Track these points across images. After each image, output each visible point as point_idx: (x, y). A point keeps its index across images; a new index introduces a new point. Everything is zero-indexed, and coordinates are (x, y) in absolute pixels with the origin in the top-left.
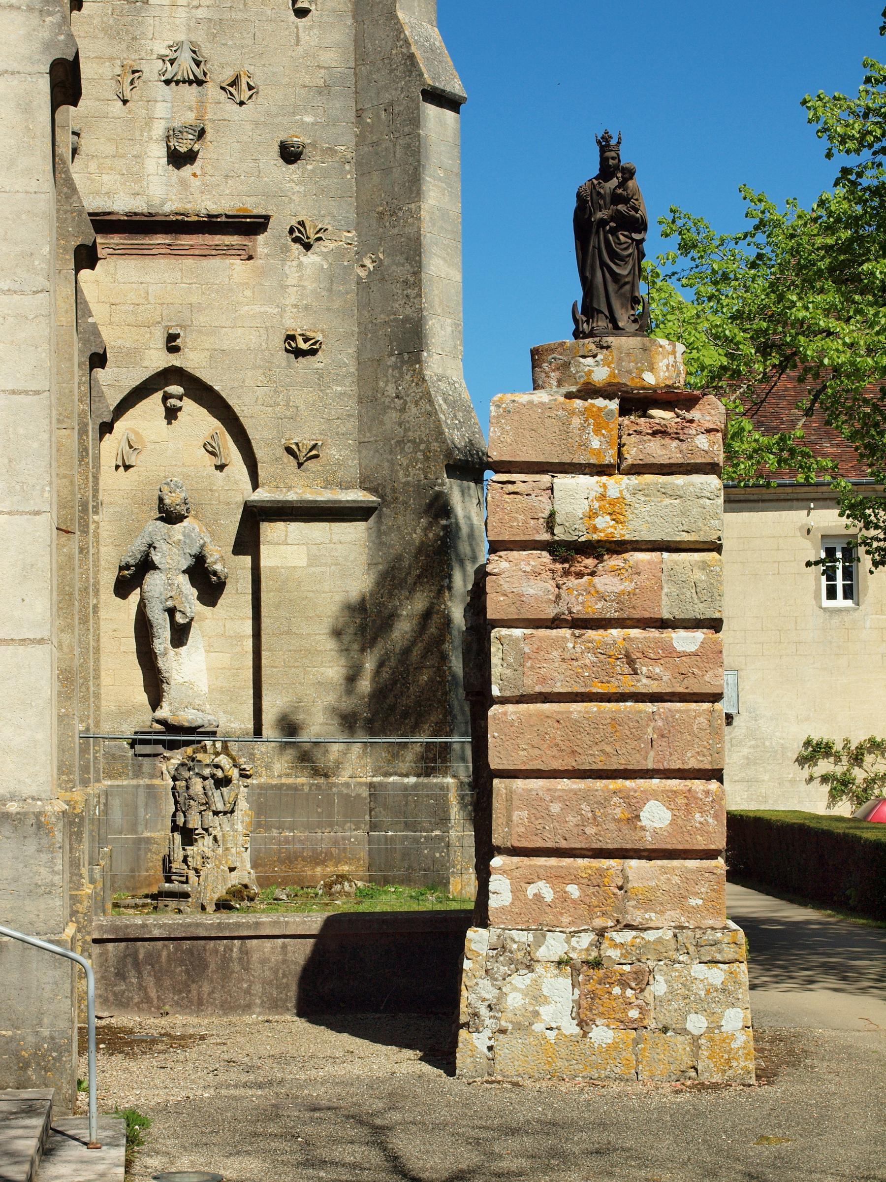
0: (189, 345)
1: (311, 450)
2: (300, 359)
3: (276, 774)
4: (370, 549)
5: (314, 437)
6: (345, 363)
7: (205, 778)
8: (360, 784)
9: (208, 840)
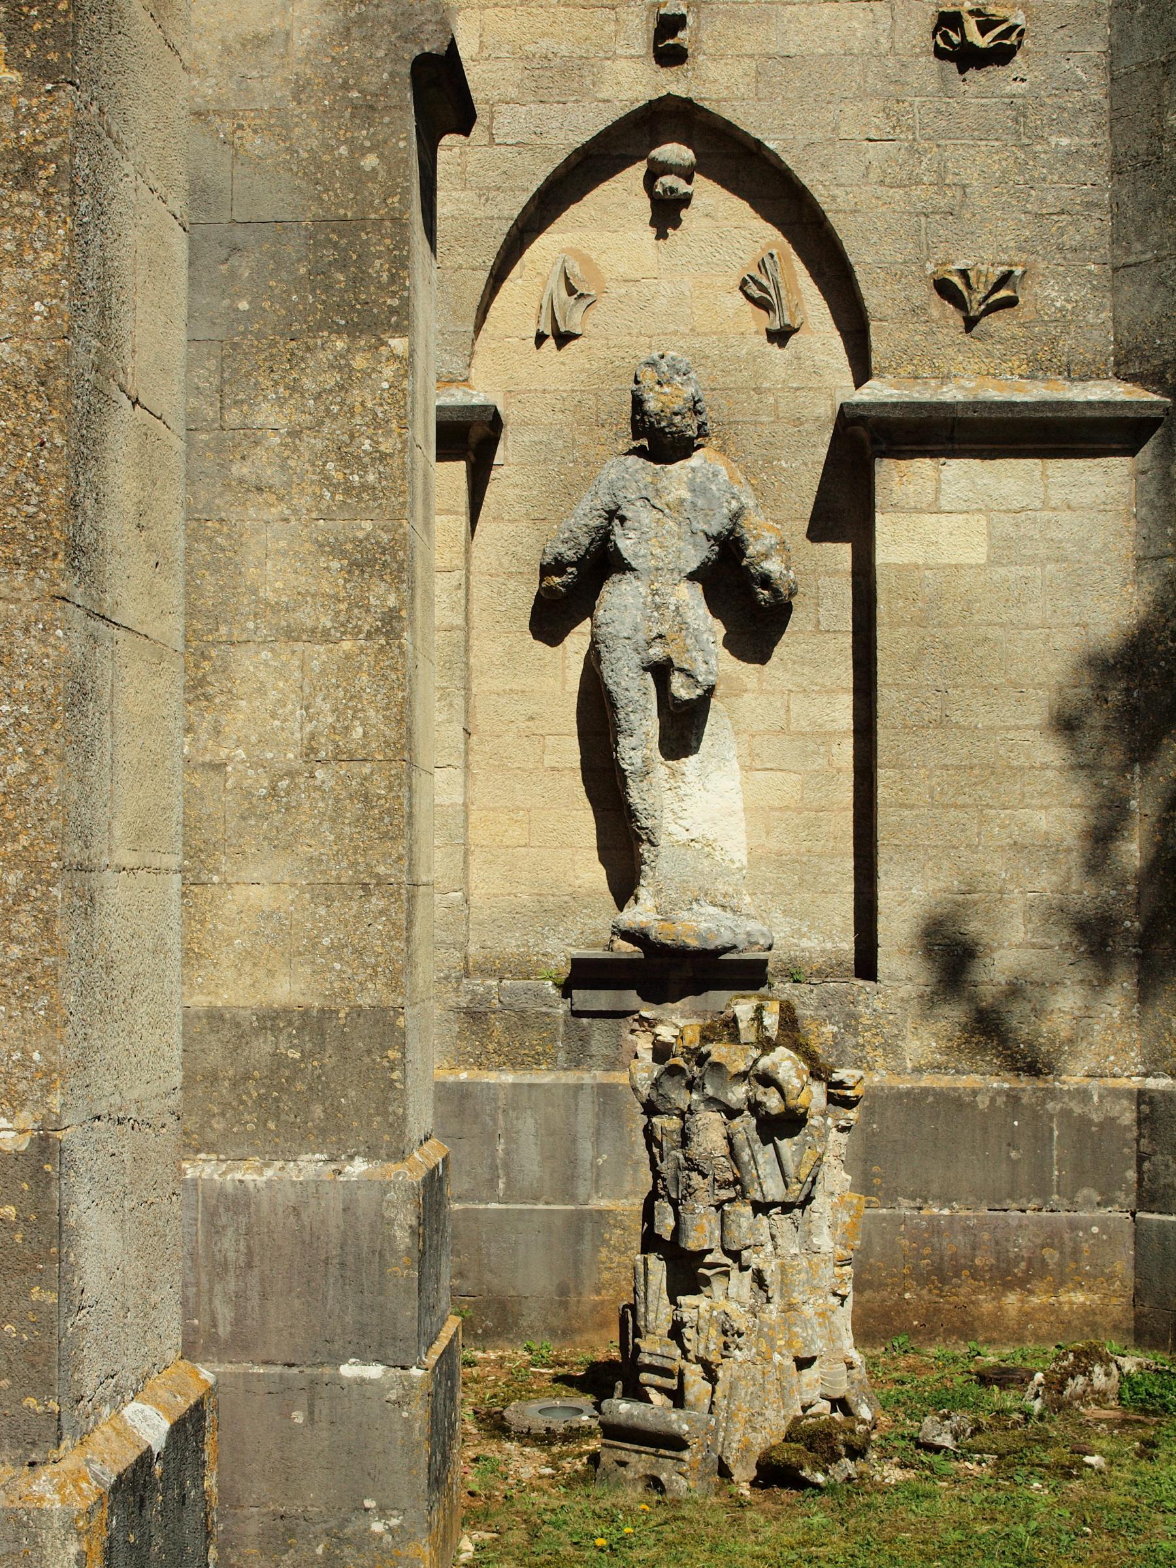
0: (708, 45)
1: (997, 287)
2: (971, 73)
3: (909, 1065)
4: (1141, 521)
5: (1005, 257)
6: (1080, 81)
7: (732, 1113)
8: (1116, 1093)
9: (741, 1283)
